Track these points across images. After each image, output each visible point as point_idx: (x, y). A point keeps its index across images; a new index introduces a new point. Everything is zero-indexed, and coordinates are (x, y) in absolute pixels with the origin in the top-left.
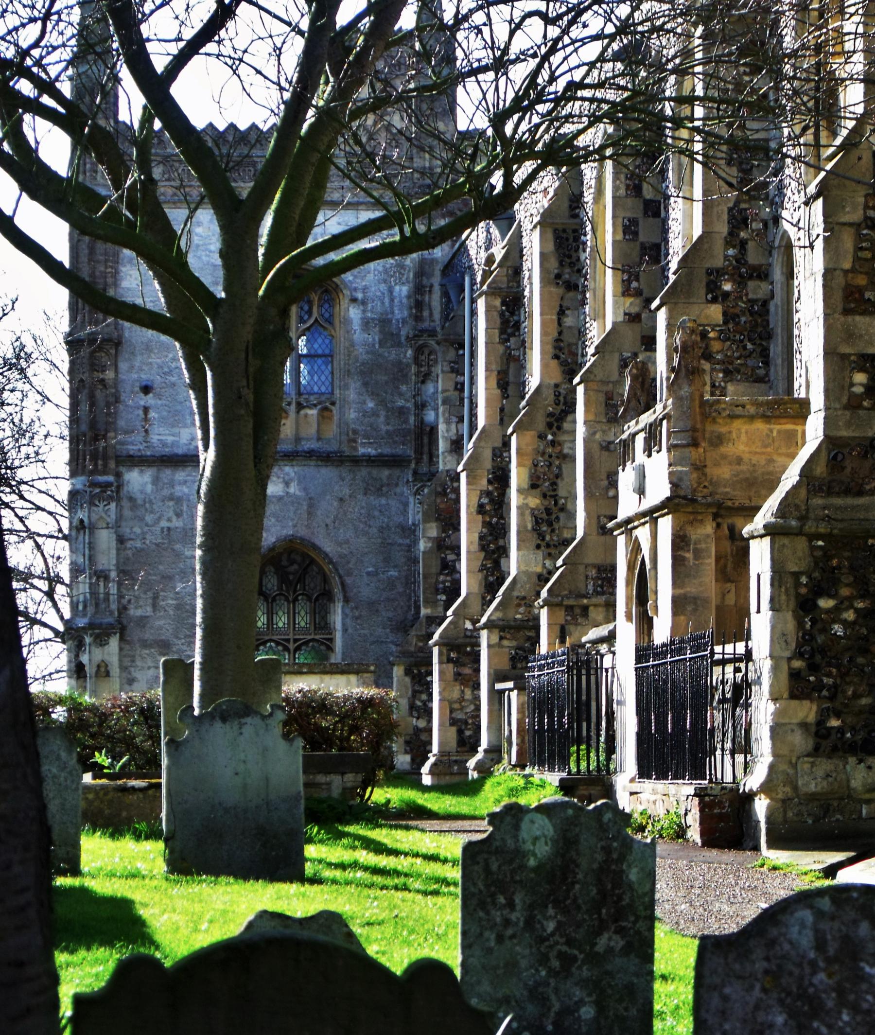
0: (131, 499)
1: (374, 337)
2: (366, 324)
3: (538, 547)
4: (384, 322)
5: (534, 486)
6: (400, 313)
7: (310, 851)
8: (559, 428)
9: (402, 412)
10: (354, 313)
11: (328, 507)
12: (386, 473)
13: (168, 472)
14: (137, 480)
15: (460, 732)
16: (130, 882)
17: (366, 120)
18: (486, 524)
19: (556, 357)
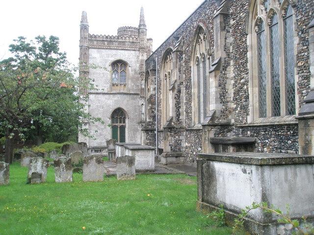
0: (91, 100)
1: (133, 73)
2: (132, 71)
3: (221, 103)
4: (135, 70)
5: (220, 86)
6: (138, 69)
7: (120, 156)
8: (226, 70)
9: (138, 86)
10: (130, 68)
11: (125, 101)
12: (135, 96)
13: (97, 95)
14: (91, 96)
15: (171, 147)
16: (165, 172)
17: (35, 168)
18: (176, 101)
19: (225, 50)
